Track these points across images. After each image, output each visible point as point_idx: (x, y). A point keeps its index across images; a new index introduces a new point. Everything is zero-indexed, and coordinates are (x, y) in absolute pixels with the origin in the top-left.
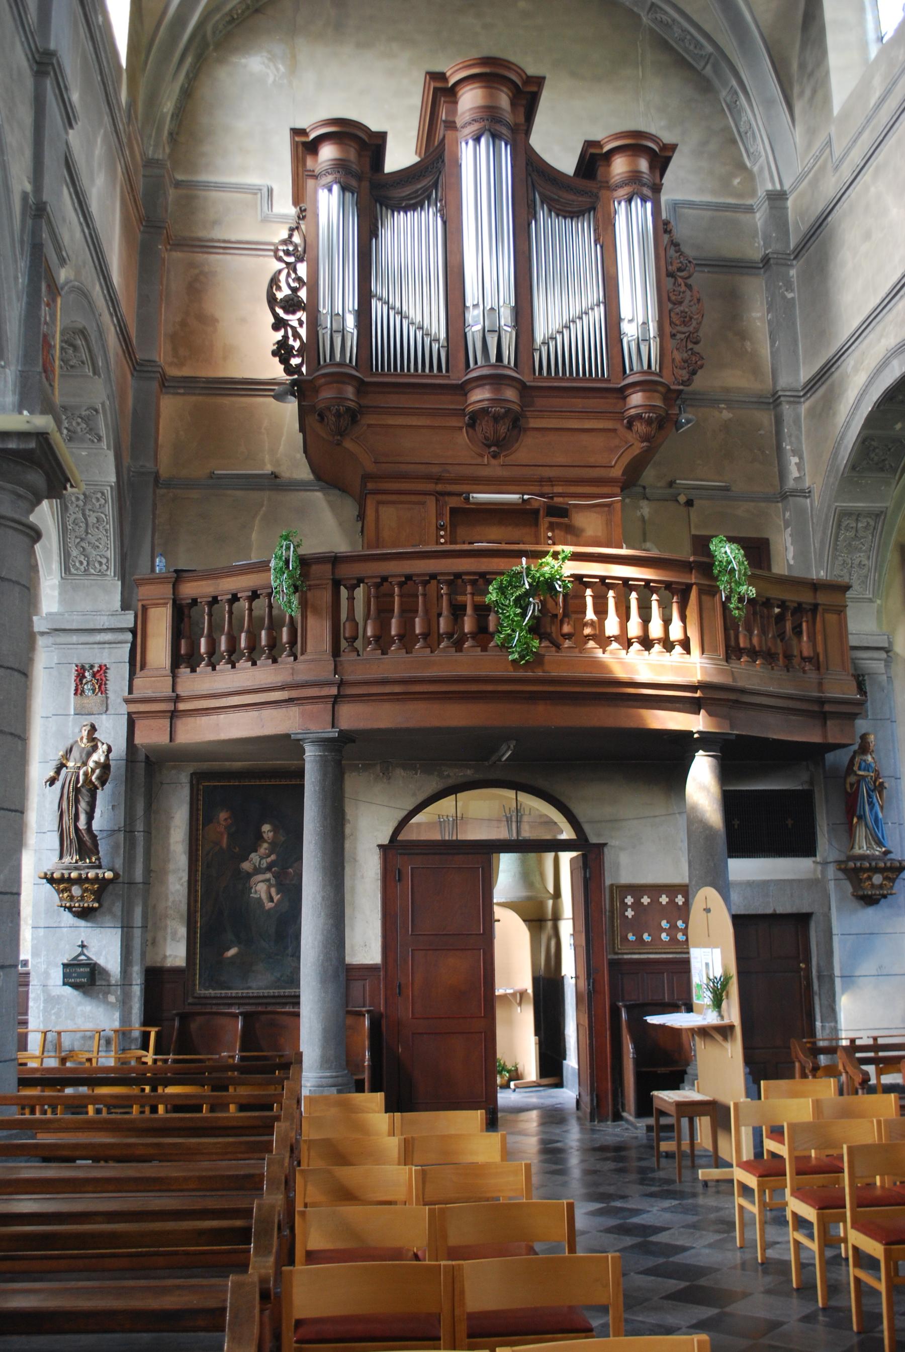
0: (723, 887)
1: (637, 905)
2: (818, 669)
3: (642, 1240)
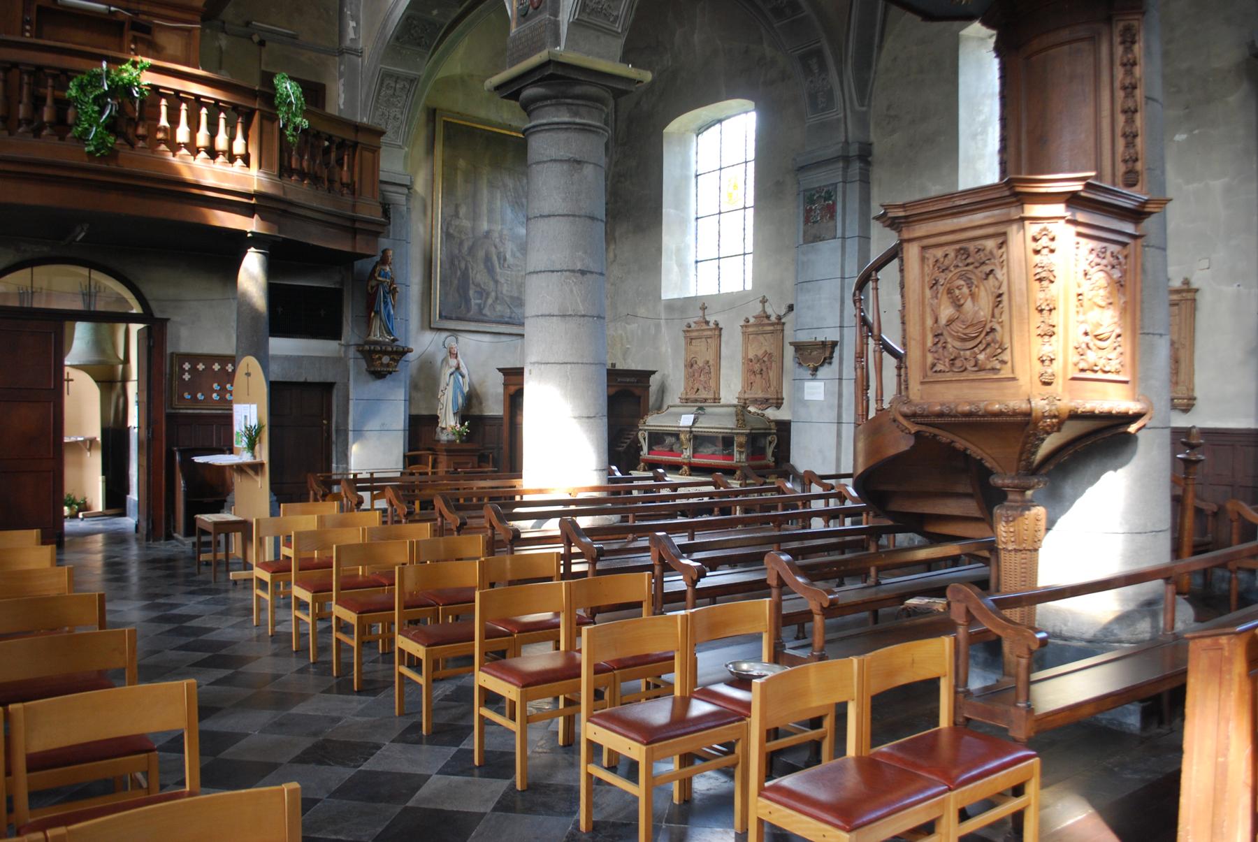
0: (264, 360)
1: (193, 370)
2: (353, 193)
3: (179, 625)
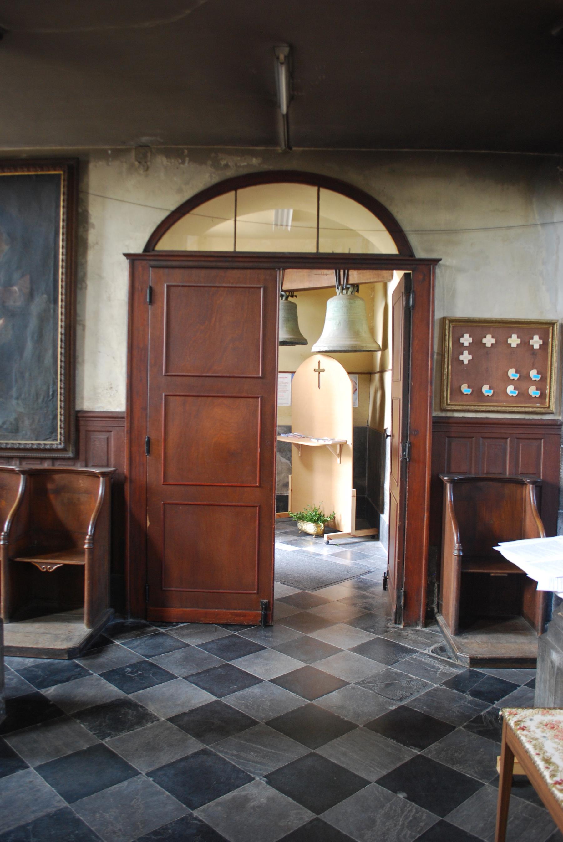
1: (477, 345)
